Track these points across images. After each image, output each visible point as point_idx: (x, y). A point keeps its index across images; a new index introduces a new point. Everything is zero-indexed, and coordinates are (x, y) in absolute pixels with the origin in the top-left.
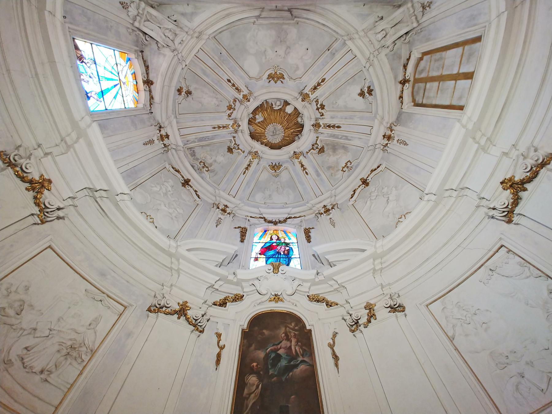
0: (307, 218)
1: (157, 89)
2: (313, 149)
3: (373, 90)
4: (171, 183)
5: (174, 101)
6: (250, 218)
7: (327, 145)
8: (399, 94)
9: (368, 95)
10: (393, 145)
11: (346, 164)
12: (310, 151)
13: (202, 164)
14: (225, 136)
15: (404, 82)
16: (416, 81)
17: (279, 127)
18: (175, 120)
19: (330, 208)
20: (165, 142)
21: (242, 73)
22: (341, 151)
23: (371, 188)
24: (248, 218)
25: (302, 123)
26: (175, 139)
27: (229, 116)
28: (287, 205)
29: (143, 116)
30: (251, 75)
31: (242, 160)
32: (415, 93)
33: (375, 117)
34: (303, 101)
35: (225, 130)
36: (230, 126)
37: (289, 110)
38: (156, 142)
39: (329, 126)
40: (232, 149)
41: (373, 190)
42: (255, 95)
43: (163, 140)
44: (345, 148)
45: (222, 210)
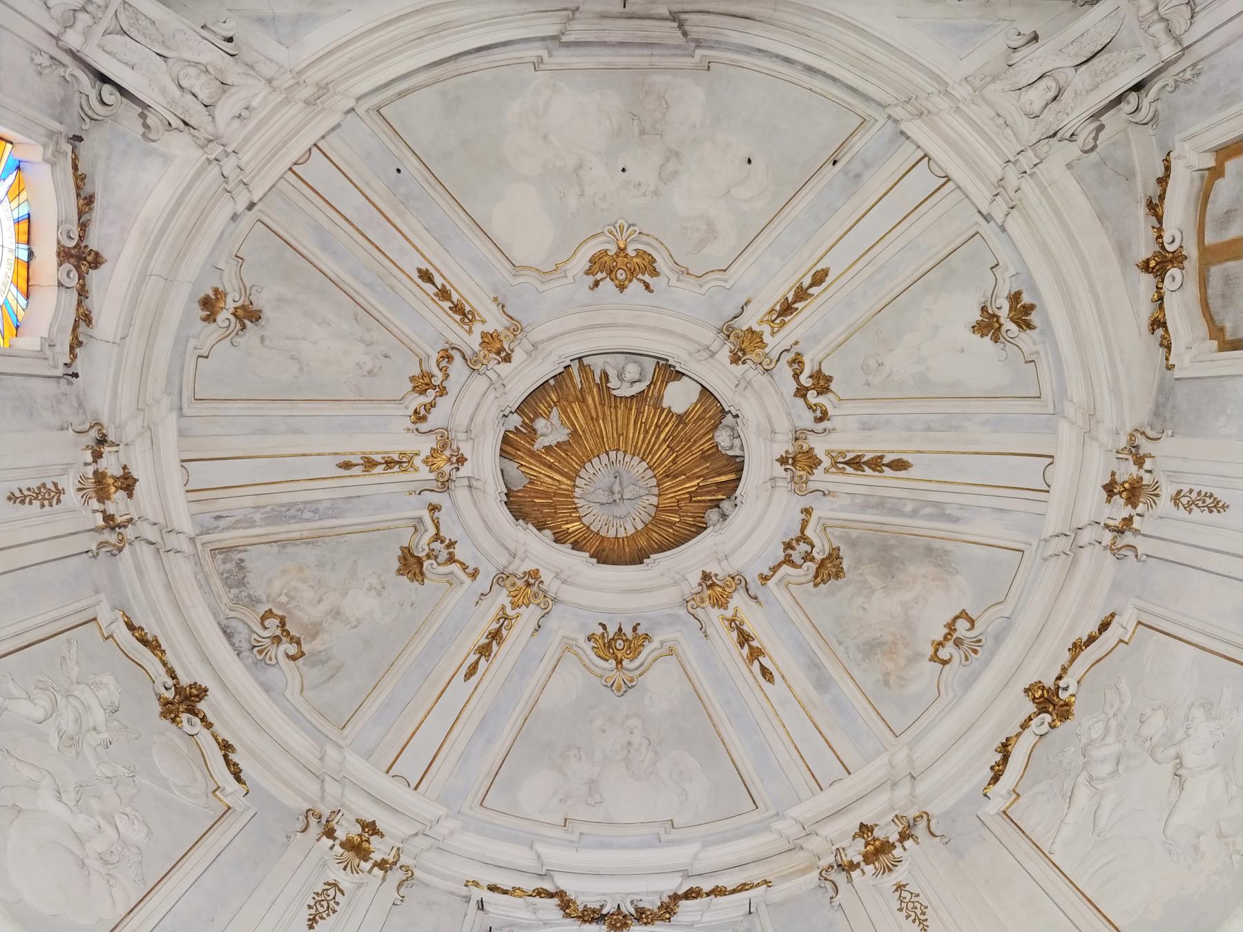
0: (778, 892)
1: (111, 289)
2: (788, 561)
3: (1032, 307)
4: (114, 691)
5: (180, 342)
6: (488, 896)
7: (853, 544)
8: (1146, 311)
9: (1013, 327)
10: (1159, 520)
11: (951, 626)
12: (774, 569)
13: (272, 623)
14: (394, 502)
15: (1160, 264)
16: (1210, 256)
17: (638, 467)
18: (172, 420)
19: (894, 838)
20: (111, 508)
21: (483, 248)
22: (918, 570)
23: (1084, 723)
24: (477, 894)
25: (737, 452)
26: (162, 497)
27: (419, 417)
28: (675, 835)
29: (31, 383)
30: (519, 257)
31: (462, 609)
32: (1215, 303)
33: (1058, 413)
34: (735, 359)
35: (395, 475)
36: (417, 461)
37: (679, 397)
38: (72, 497)
39: (856, 463)
40: (420, 562)
41: (1096, 733)
42: (536, 335)
43: (103, 496)
44: (936, 556)
45: (349, 845)
